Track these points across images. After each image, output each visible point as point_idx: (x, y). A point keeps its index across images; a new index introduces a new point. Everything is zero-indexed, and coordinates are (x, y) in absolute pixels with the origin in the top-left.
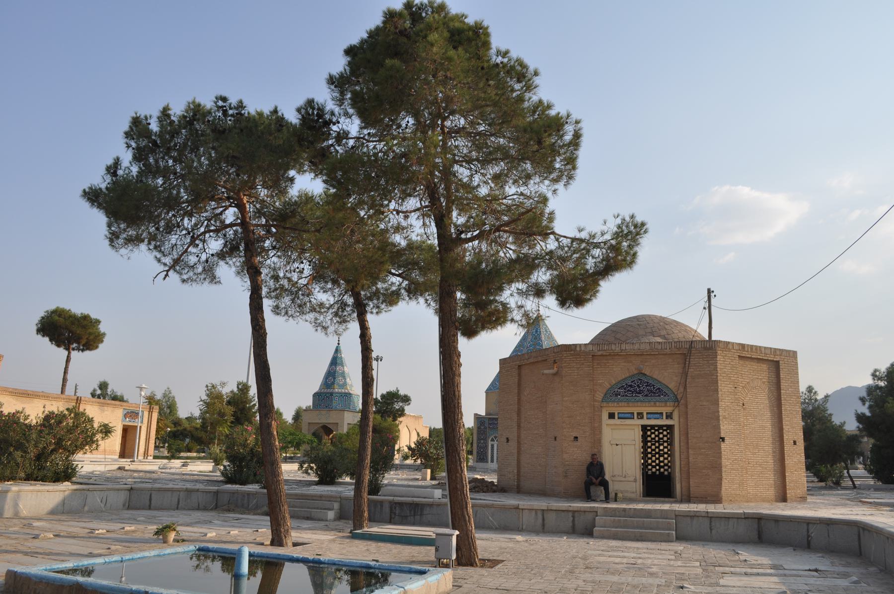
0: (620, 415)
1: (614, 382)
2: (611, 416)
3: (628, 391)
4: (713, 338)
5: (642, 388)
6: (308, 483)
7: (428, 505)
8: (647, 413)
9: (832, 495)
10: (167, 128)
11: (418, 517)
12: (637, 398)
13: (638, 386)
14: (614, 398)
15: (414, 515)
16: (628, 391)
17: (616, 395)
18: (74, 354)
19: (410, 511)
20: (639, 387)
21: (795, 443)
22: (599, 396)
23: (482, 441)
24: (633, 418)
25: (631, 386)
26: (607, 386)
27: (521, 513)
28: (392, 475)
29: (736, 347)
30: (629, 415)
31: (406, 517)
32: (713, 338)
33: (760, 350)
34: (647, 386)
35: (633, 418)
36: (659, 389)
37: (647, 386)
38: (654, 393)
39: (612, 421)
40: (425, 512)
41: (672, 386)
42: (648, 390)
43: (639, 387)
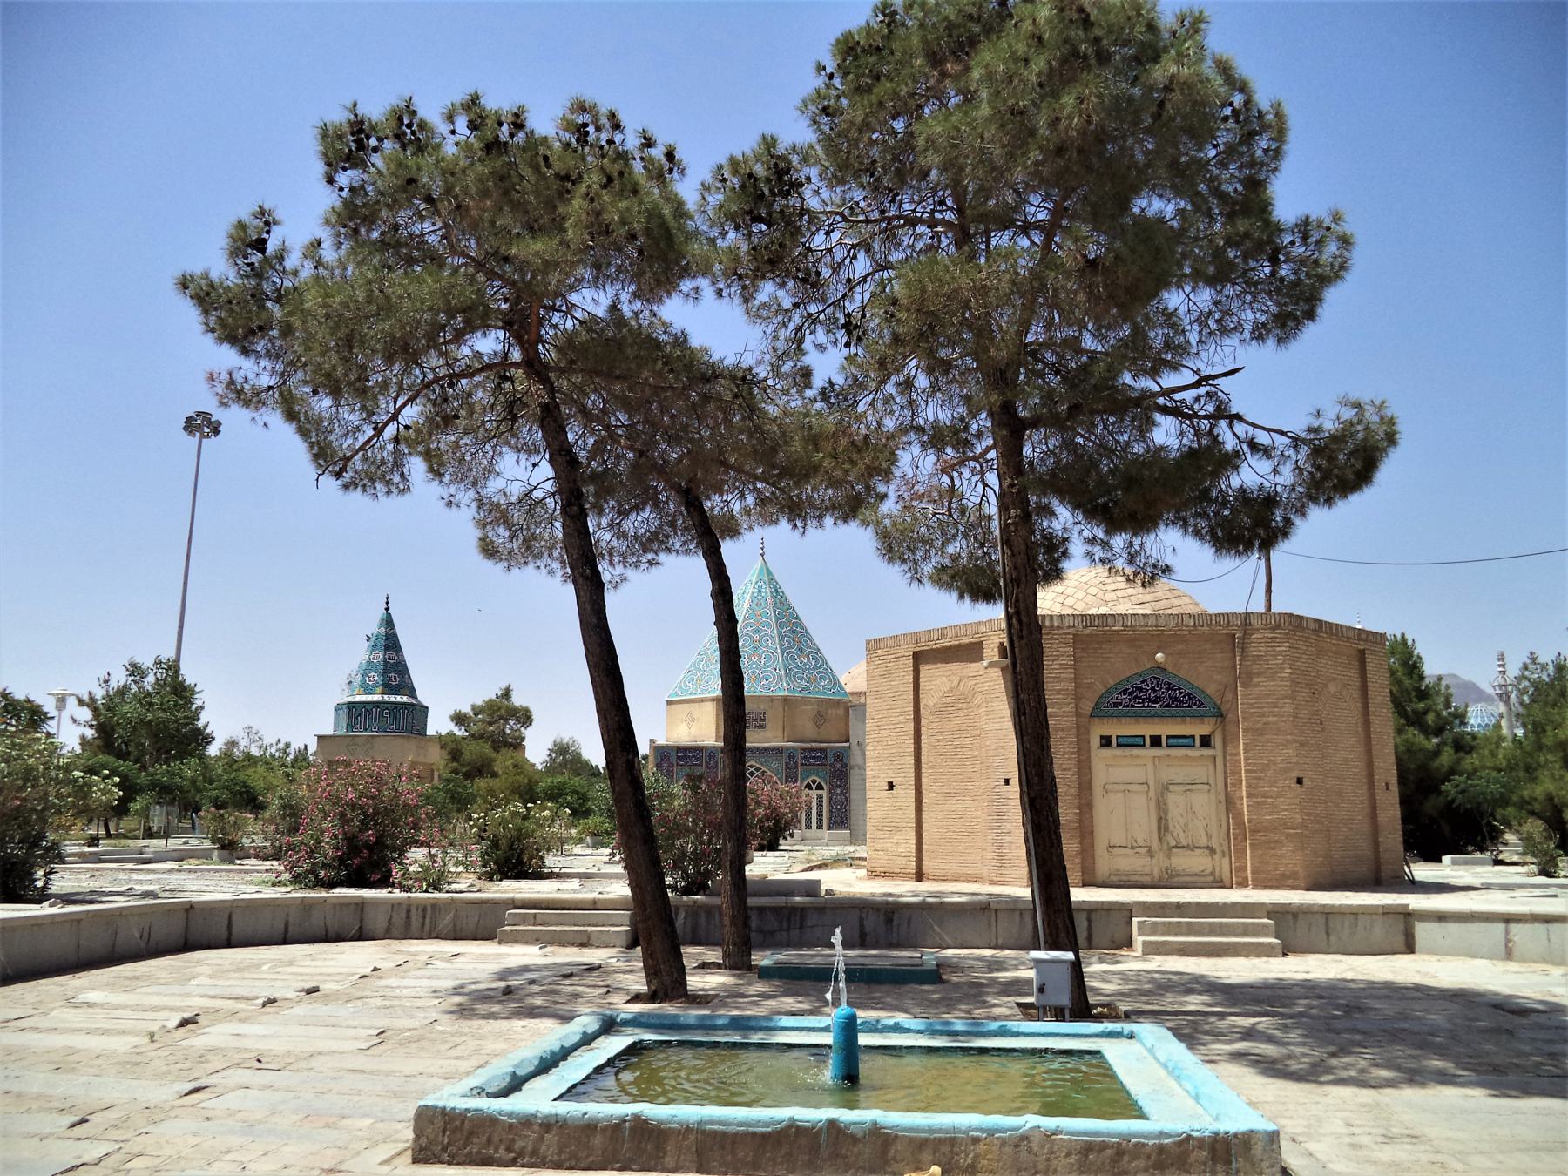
0: (1120, 740)
1: (1112, 683)
2: (1106, 742)
3: (1136, 697)
4: (1275, 609)
5: (1159, 694)
6: (1290, 882)
7: (816, 909)
8: (1168, 737)
9: (1030, 871)
10: (957, 106)
11: (795, 933)
12: (1153, 711)
13: (1153, 689)
14: (1111, 710)
15: (788, 930)
16: (1136, 697)
17: (1116, 705)
18: (1258, 606)
19: (781, 922)
20: (1155, 691)
21: (1007, 782)
22: (1087, 707)
23: (839, 791)
24: (1144, 745)
25: (1140, 689)
26: (1100, 689)
27: (993, 919)
28: (104, 845)
29: (1312, 626)
30: (1175, 741)
31: (772, 933)
32: (1275, 609)
33: (1331, 629)
34: (1168, 689)
35: (1144, 745)
36: (1189, 694)
37: (1168, 689)
38: (1181, 701)
39: (1106, 752)
40: (809, 923)
41: (1211, 689)
42: (1170, 697)
43: (1155, 691)
